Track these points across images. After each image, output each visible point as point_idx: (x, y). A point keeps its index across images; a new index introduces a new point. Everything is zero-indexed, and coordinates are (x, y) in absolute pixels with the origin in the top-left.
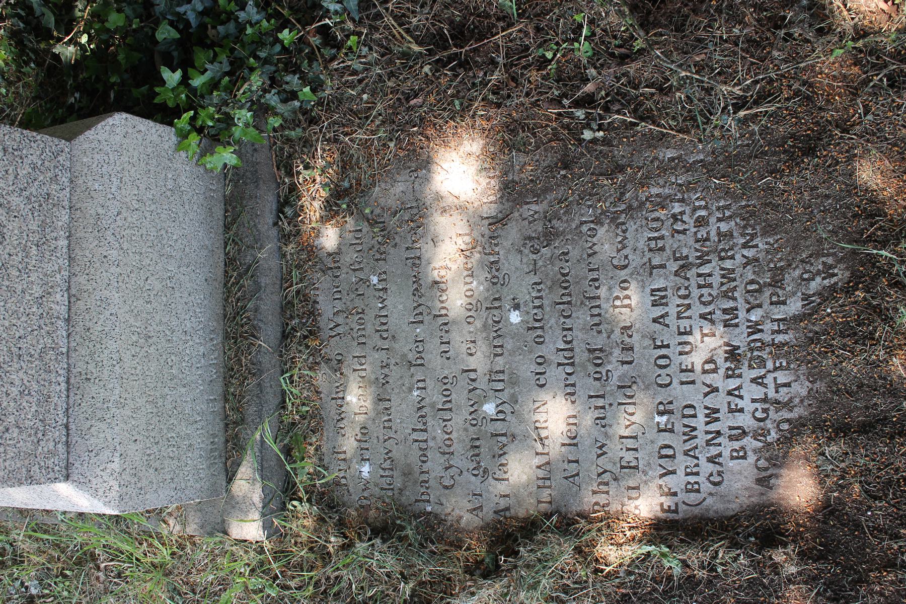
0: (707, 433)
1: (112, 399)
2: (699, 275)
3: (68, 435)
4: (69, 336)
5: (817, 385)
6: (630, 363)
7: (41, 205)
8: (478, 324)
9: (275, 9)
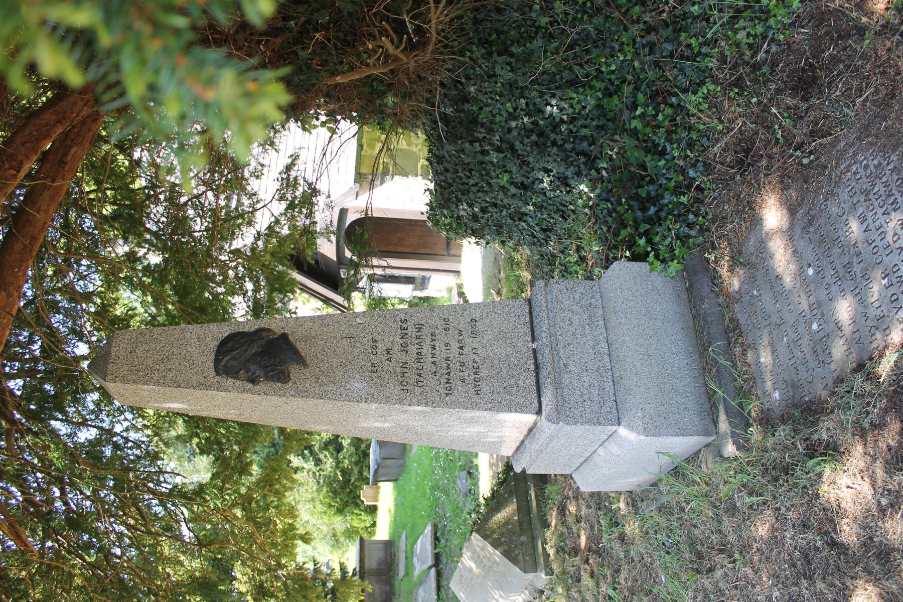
2: (874, 194)
6: (862, 261)
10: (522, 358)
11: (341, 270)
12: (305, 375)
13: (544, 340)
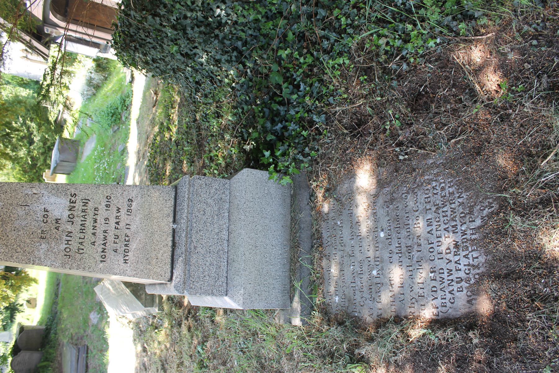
0: (448, 280)
2: (443, 212)
5: (488, 257)
8: (371, 238)
10: (164, 236)
13: (182, 225)
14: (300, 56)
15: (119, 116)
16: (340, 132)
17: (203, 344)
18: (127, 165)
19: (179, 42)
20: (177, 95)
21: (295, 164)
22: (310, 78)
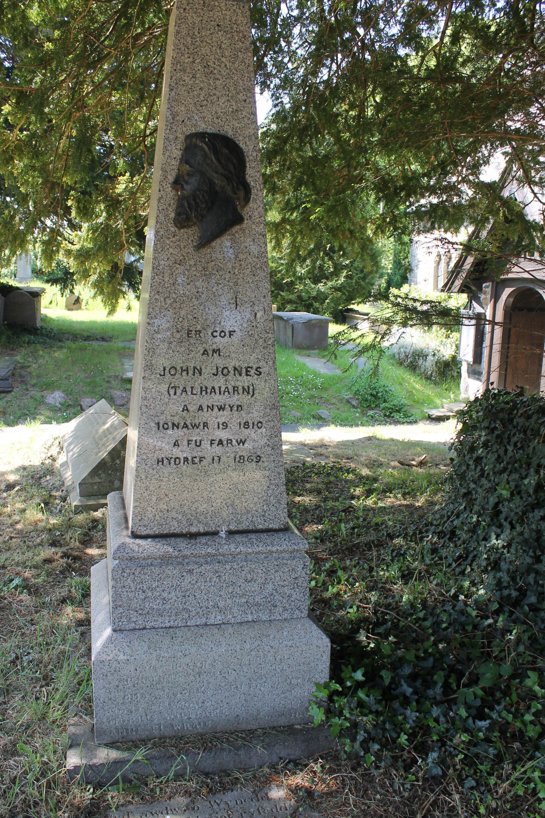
1: (162, 652)
3: (139, 629)
4: (197, 626)
7: (269, 602)
9: (419, 733)
11: (491, 283)
12: (185, 247)
13: (226, 547)
14: (534, 714)
15: (373, 406)
16: (415, 807)
17: (24, 588)
18: (300, 428)
19: (517, 498)
20: (427, 501)
21: (347, 727)
22: (500, 737)
